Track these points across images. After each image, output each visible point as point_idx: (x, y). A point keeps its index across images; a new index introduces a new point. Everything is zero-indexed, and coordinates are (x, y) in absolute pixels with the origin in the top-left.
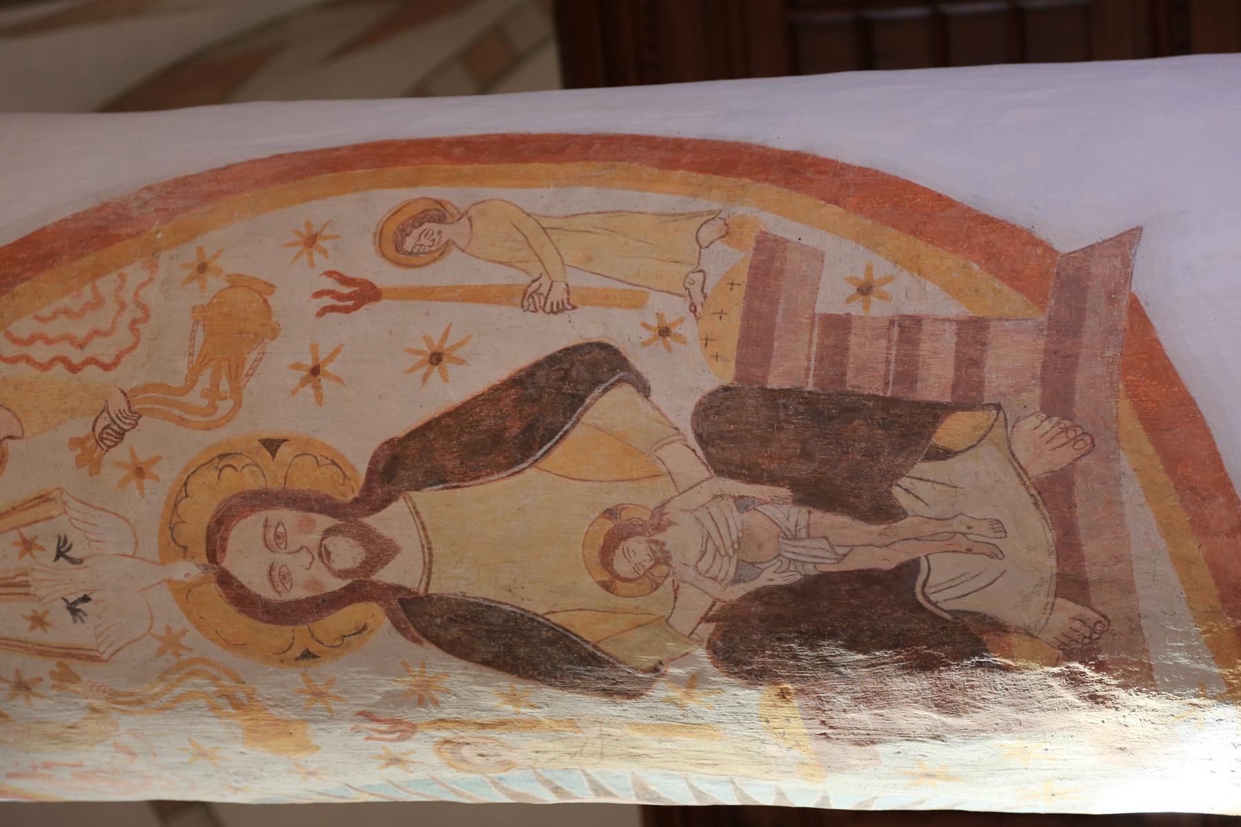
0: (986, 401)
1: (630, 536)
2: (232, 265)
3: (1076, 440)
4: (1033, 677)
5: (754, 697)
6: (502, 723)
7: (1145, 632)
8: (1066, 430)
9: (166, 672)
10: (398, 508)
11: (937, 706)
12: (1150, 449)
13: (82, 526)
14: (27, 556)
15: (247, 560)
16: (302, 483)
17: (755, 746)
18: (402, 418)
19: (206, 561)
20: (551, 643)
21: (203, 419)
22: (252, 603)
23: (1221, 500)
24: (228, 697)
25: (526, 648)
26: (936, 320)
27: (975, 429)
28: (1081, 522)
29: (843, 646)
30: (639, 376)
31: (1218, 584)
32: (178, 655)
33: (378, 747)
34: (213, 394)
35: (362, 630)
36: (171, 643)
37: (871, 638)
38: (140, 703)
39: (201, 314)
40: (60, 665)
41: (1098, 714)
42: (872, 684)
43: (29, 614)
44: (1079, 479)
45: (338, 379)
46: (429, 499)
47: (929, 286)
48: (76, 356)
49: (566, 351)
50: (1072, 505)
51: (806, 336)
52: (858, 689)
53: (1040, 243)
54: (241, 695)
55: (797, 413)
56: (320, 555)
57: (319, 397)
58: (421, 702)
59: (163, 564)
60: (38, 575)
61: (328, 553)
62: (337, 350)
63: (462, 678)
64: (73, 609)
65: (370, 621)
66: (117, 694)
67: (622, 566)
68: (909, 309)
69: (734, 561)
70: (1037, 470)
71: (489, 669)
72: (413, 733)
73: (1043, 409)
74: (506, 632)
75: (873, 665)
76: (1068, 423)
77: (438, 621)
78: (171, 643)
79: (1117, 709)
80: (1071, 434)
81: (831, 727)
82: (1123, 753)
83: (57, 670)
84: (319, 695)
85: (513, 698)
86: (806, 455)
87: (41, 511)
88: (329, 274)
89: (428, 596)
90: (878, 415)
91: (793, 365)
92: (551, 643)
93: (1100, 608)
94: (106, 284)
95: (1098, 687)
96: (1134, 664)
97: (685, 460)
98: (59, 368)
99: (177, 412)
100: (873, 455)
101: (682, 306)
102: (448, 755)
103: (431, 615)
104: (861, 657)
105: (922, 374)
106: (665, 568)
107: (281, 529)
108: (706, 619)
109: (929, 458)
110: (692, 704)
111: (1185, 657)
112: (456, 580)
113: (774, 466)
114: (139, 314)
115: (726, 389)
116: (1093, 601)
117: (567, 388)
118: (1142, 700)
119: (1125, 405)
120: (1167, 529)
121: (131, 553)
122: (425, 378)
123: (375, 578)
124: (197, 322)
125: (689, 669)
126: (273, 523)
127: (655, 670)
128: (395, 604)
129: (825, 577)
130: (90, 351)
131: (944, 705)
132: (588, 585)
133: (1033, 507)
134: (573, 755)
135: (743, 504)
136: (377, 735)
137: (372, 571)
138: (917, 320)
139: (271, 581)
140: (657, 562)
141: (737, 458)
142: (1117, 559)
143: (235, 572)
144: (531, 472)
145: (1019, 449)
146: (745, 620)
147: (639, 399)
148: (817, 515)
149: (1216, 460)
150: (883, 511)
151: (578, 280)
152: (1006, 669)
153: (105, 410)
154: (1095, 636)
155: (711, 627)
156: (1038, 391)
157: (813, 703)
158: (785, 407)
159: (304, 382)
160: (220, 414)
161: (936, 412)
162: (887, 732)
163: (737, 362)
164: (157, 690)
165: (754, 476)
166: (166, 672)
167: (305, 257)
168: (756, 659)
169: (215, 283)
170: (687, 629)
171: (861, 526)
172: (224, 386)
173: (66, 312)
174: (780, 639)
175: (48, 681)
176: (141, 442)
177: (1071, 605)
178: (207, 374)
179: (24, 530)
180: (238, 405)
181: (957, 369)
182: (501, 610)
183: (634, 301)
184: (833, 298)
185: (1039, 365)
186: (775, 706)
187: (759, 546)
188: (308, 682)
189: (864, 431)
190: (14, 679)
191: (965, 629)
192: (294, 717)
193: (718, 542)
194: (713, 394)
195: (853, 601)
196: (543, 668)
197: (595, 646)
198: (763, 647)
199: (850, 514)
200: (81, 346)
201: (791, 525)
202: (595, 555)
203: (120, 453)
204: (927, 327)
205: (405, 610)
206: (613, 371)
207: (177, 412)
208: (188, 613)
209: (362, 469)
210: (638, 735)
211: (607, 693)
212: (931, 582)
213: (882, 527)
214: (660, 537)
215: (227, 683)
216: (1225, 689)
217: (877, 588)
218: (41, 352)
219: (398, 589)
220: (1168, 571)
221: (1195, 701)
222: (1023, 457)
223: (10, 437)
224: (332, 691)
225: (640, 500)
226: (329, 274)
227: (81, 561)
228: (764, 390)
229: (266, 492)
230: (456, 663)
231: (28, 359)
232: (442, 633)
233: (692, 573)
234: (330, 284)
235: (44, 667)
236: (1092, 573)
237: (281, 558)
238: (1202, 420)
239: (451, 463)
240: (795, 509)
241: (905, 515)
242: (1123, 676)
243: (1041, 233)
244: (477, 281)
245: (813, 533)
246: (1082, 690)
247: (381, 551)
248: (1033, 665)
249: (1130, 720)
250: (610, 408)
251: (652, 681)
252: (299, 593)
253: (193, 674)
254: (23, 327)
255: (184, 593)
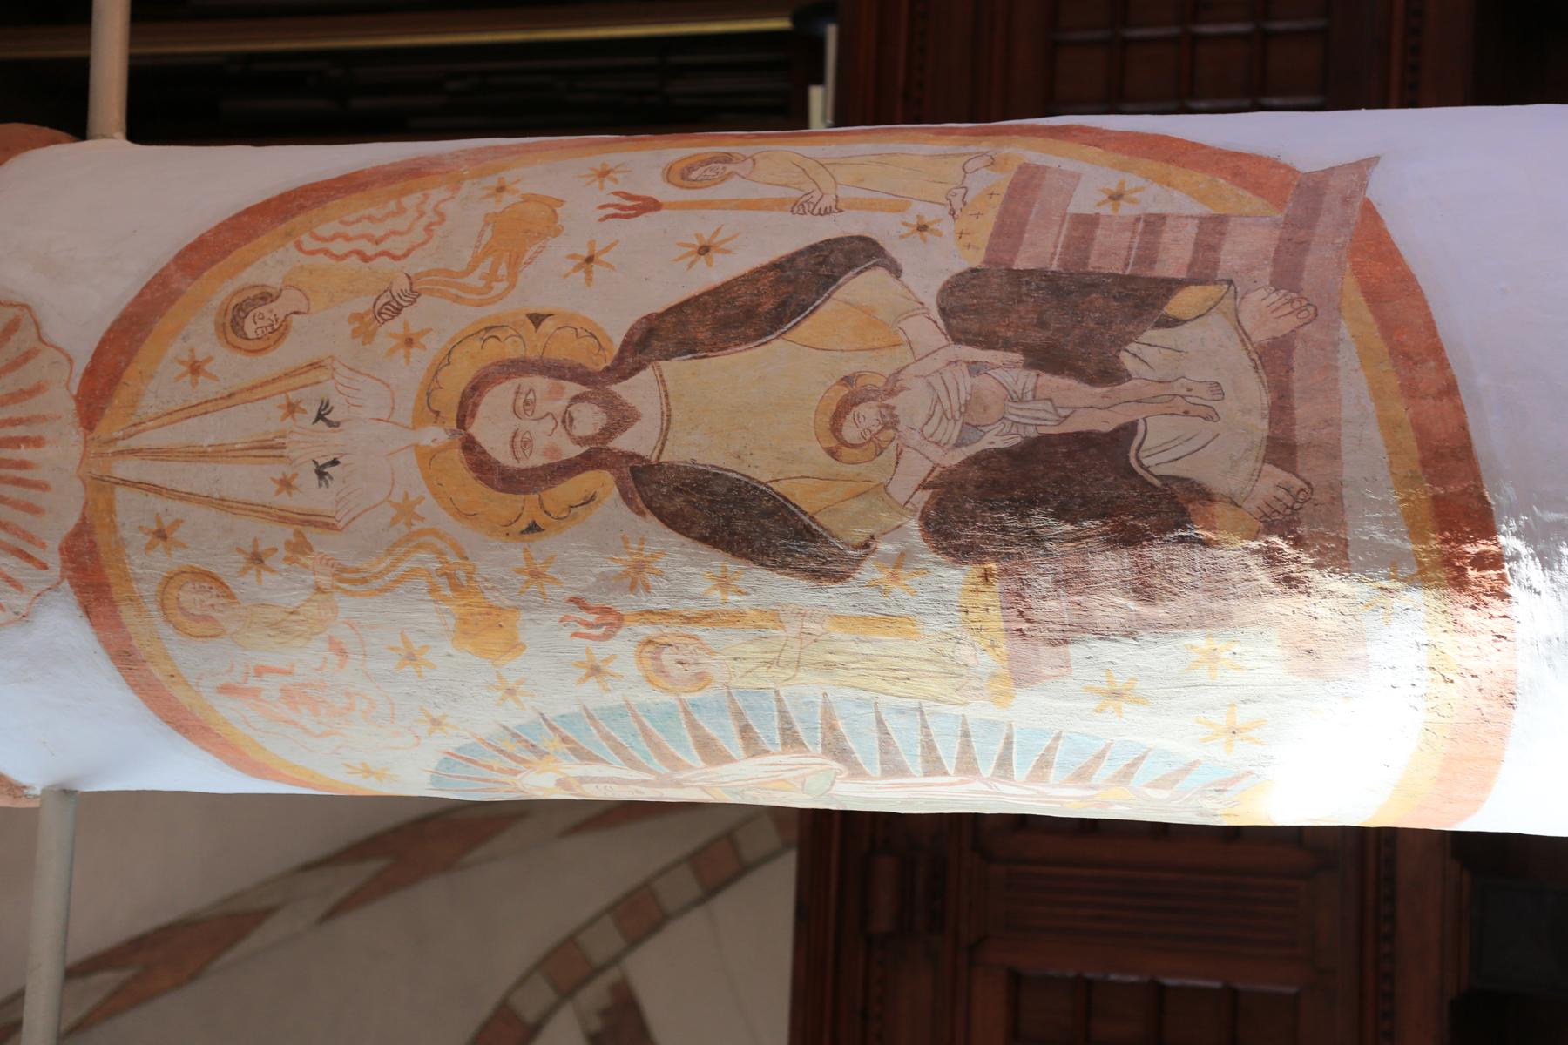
0: (1219, 277)
1: (863, 401)
2: (527, 188)
3: (1300, 310)
4: (1232, 554)
5: (955, 578)
6: (708, 616)
7: (1346, 502)
8: (1292, 301)
9: (396, 545)
10: (646, 376)
11: (1135, 591)
12: (1369, 318)
13: (345, 390)
14: (289, 419)
15: (493, 430)
16: (558, 353)
17: (948, 647)
18: (660, 298)
19: (454, 426)
20: (768, 514)
21: (476, 297)
22: (491, 469)
23: (1432, 364)
24: (449, 576)
25: (743, 521)
26: (1180, 217)
27: (1206, 300)
28: (1296, 386)
29: (1053, 515)
30: (893, 261)
31: (1421, 448)
32: (410, 525)
33: (582, 649)
34: (491, 277)
35: (589, 500)
36: (406, 511)
37: (1081, 505)
38: (364, 581)
39: (490, 219)
40: (298, 534)
41: (1289, 601)
42: (1074, 563)
43: (279, 476)
44: (1299, 344)
45: (610, 266)
46: (677, 369)
47: (1176, 194)
48: (370, 249)
49: (828, 241)
50: (1290, 369)
51: (1056, 229)
52: (1060, 569)
53: (1285, 166)
54: (461, 574)
55: (1039, 288)
56: (564, 422)
57: (589, 280)
58: (633, 588)
59: (414, 428)
60: (296, 437)
61: (572, 419)
62: (613, 245)
63: (678, 557)
64: (321, 474)
65: (600, 490)
66: (345, 570)
67: (850, 432)
68: (1155, 210)
69: (959, 425)
70: (1260, 336)
71: (705, 547)
72: (619, 627)
73: (1272, 284)
74: (728, 503)
75: (1078, 539)
76: (1294, 295)
77: (665, 490)
78: (406, 511)
79: (1309, 595)
80: (1296, 305)
81: (1028, 621)
82: (1309, 658)
83: (293, 539)
84: (536, 575)
85: (723, 583)
86: (1042, 324)
87: (312, 375)
88: (616, 193)
89: (659, 464)
90: (1115, 290)
91: (1040, 250)
92: (768, 514)
93: (1305, 475)
94: (410, 201)
95: (1293, 566)
96: (1331, 539)
97: (927, 332)
98: (354, 258)
99: (454, 291)
100: (1104, 324)
101: (942, 211)
102: (648, 663)
103: (659, 483)
104: (1068, 527)
105: (1162, 256)
106: (891, 432)
107: (531, 396)
108: (924, 486)
109: (1158, 326)
110: (896, 589)
111: (1381, 531)
112: (692, 448)
113: (1010, 334)
114: (436, 219)
115: (973, 270)
116: (1299, 467)
117: (823, 270)
118: (1336, 584)
119: (1350, 281)
120: (1377, 393)
121: (384, 415)
122: (691, 265)
123: (610, 445)
124: (487, 224)
125: (898, 545)
126: (525, 389)
127: (866, 546)
128: (626, 472)
129: (1045, 440)
130: (383, 246)
131: (1144, 592)
132: (815, 451)
133: (1252, 371)
134: (769, 663)
135: (975, 368)
136: (585, 630)
137: (610, 438)
138: (1162, 218)
139: (513, 447)
140: (885, 427)
141: (975, 327)
142: (1327, 422)
143: (479, 438)
144: (779, 342)
145: (1245, 318)
146: (961, 487)
147: (890, 279)
148: (1046, 378)
149: (1431, 327)
150: (1109, 375)
151: (844, 193)
152: (1206, 543)
153: (389, 290)
154: (1297, 506)
155: (927, 495)
156: (1269, 270)
157: (1014, 587)
158: (1028, 283)
159: (577, 268)
160: (493, 293)
161: (1171, 286)
162: (1082, 628)
163: (988, 250)
164: (383, 566)
165: (989, 343)
166: (396, 545)
167: (597, 183)
168: (967, 532)
169: (508, 199)
170: (902, 498)
171: (1086, 389)
172: (503, 270)
173: (370, 218)
174: (991, 509)
175: (283, 552)
176: (413, 318)
177: (1277, 471)
178: (488, 262)
179: (291, 394)
180: (512, 286)
181: (1195, 252)
182: (727, 478)
183: (899, 207)
184: (1085, 201)
185: (1272, 250)
186: (977, 591)
187: (986, 409)
188: (528, 558)
189: (1100, 302)
190: (250, 550)
191: (1173, 497)
192: (508, 603)
193: (946, 404)
194: (961, 275)
195: (1070, 465)
196: (757, 545)
197: (811, 518)
198: (974, 517)
199: (1076, 377)
200: (377, 243)
201: (1019, 388)
202: (826, 420)
203: (395, 325)
204: (1170, 221)
205: (635, 479)
206: (869, 257)
207: (454, 291)
208: (427, 478)
209: (618, 341)
210: (837, 633)
211: (816, 575)
212: (1147, 445)
213: (1105, 389)
214: (890, 402)
215: (451, 558)
216: (1416, 569)
217: (1092, 451)
218: (339, 247)
219: (632, 456)
220: (1374, 434)
221: (1385, 584)
222: (1248, 325)
223: (296, 313)
224: (550, 571)
225: (875, 367)
226: (616, 193)
227: (338, 424)
228: (1010, 270)
229: (524, 361)
230: (675, 538)
231: (327, 252)
232: (666, 504)
233: (917, 437)
234: (616, 200)
235: (277, 536)
236: (1301, 435)
237: (527, 425)
238: (1421, 293)
239: (703, 335)
240: (1026, 372)
241: (1129, 377)
242: (1319, 553)
243: (1284, 160)
244: (755, 196)
245: (1038, 395)
246: (1277, 571)
247: (621, 418)
248: (1234, 538)
249: (1320, 611)
250: (861, 287)
251: (860, 560)
252: (537, 460)
253: (419, 547)
254: (325, 230)
255: (428, 458)
